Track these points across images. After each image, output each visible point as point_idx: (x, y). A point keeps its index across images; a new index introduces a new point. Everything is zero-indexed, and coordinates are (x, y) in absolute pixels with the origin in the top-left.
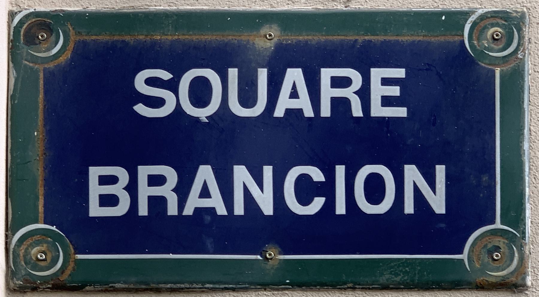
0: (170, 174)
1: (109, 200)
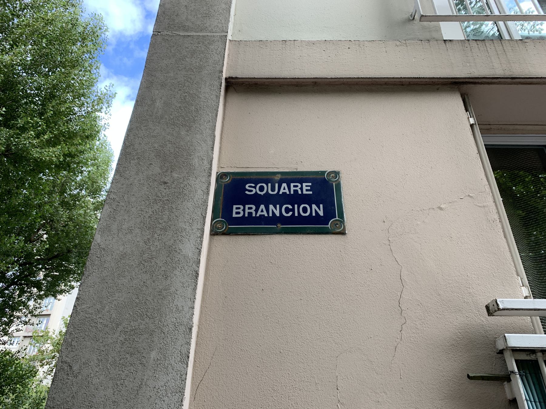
0: (254, 207)
1: (238, 213)
